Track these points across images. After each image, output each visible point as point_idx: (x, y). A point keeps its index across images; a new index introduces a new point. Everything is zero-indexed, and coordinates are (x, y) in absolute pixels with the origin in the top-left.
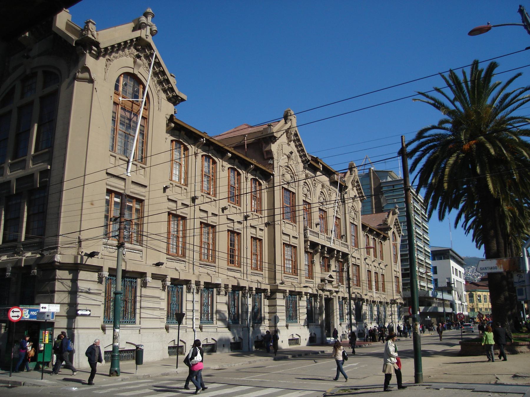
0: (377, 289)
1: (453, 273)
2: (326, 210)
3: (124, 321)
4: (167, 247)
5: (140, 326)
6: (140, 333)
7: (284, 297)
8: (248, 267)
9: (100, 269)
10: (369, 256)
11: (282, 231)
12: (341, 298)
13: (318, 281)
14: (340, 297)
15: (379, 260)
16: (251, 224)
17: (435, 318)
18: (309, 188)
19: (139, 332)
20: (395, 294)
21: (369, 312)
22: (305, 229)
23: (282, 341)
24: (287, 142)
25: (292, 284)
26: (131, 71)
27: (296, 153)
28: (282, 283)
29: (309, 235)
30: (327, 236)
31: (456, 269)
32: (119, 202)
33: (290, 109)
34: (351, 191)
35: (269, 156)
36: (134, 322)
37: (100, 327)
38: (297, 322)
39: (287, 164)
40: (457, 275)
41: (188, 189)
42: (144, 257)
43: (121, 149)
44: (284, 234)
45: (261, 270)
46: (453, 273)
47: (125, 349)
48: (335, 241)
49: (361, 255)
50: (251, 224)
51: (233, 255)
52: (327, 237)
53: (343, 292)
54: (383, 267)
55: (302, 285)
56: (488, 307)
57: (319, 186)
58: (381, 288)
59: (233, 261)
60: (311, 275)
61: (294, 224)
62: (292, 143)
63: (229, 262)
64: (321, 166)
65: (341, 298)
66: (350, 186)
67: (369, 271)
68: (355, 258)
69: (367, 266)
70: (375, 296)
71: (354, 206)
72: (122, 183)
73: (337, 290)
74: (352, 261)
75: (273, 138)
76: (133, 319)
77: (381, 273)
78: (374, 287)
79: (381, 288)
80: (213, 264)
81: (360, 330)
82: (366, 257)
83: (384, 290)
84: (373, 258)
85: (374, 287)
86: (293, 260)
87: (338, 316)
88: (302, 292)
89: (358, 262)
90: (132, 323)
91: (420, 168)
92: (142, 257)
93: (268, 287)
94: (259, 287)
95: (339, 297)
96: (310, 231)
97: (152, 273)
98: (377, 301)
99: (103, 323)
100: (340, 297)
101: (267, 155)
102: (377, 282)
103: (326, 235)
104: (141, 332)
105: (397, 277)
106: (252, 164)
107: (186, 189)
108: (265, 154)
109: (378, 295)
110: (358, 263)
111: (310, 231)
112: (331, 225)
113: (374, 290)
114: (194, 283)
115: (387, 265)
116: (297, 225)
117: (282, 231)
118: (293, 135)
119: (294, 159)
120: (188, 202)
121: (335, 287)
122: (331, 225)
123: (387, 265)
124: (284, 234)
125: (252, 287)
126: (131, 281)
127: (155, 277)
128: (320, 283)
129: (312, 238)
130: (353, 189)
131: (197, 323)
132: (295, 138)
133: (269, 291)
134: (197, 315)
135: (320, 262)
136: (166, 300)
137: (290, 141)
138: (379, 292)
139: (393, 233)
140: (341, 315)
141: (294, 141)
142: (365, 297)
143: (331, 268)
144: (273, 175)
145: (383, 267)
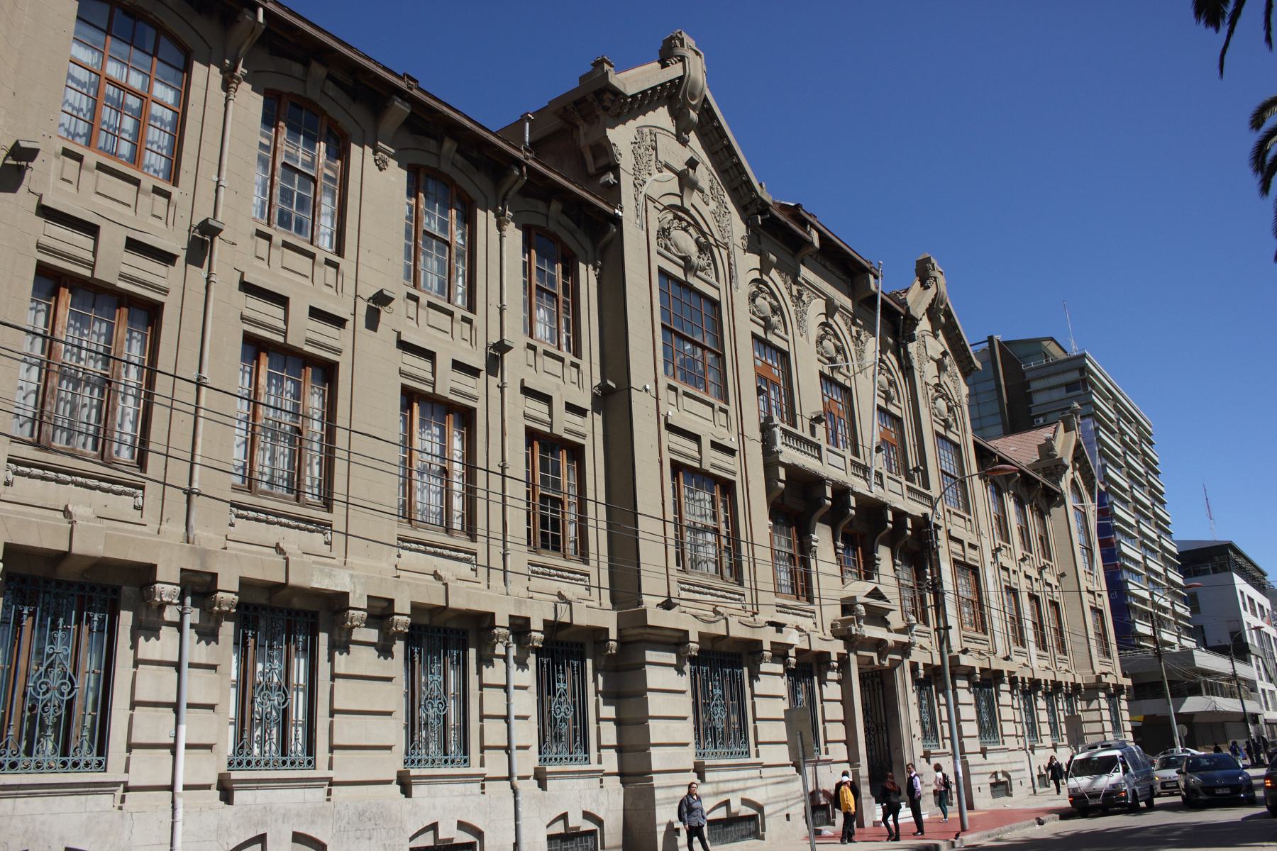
0: (1042, 644)
1: (1245, 609)
2: (848, 384)
4: (529, 530)
5: (482, 771)
6: (602, 787)
8: (197, 468)
10: (1006, 544)
11: (666, 419)
12: (921, 666)
13: (833, 613)
14: (917, 663)
15: (1037, 557)
16: (523, 381)
17: (612, 705)
18: (841, 342)
19: (599, 785)
20: (1096, 660)
21: (1023, 713)
22: (766, 428)
25: (715, 611)
26: (677, 201)
27: (705, 174)
28: (668, 605)
29: (779, 446)
30: (855, 459)
31: (1251, 600)
32: (818, 524)
33: (928, 255)
34: (930, 340)
35: (602, 162)
36: (465, 761)
37: (532, 773)
38: (748, 754)
39: (936, 381)
40: (1254, 613)
41: (478, 319)
42: (819, 624)
44: (672, 428)
45: (583, 555)
46: (1245, 609)
48: (885, 478)
49: (979, 535)
50: (523, 381)
51: (555, 523)
52: (909, 488)
53: (925, 652)
54: (1053, 580)
55: (763, 618)
56: (258, 423)
57: (818, 306)
58: (1051, 640)
59: (556, 539)
60: (803, 587)
61: (967, 516)
64: (815, 235)
65: (921, 666)
66: (924, 325)
67: (1012, 591)
68: (960, 542)
69: (1004, 574)
70: (1035, 666)
71: (942, 383)
73: (904, 638)
74: (951, 552)
76: (94, 758)
77: (1048, 598)
78: (1030, 634)
79: (1051, 640)
80: (322, 515)
82: (997, 546)
83: (1062, 647)
84: (1019, 552)
85: (1030, 634)
86: (723, 533)
87: (917, 730)
88: (759, 642)
89: (973, 557)
90: (266, 765)
92: (815, 624)
93: (608, 620)
94: (565, 618)
95: (914, 666)
96: (785, 432)
97: (182, 570)
99: (224, 769)
100: (917, 663)
101: (595, 157)
102: (1039, 625)
103: (905, 483)
104: (486, 790)
105: (1097, 612)
106: (519, 163)
107: (167, 195)
108: (589, 158)
109: (1045, 663)
110: (971, 559)
111: (785, 432)
112: (870, 430)
113: (1032, 646)
114: (541, 627)
115: (1063, 575)
116: (732, 409)
117: (666, 419)
119: (707, 191)
120: (479, 362)
121: (898, 631)
122: (870, 430)
123: (1063, 575)
124: (672, 428)
125: (493, 614)
128: (840, 617)
129: (790, 455)
131: (527, 762)
133: (613, 634)
134: (527, 733)
139: (1073, 482)
140: (928, 726)
142: (768, 637)
143: (880, 567)
144: (618, 221)
145: (1053, 580)
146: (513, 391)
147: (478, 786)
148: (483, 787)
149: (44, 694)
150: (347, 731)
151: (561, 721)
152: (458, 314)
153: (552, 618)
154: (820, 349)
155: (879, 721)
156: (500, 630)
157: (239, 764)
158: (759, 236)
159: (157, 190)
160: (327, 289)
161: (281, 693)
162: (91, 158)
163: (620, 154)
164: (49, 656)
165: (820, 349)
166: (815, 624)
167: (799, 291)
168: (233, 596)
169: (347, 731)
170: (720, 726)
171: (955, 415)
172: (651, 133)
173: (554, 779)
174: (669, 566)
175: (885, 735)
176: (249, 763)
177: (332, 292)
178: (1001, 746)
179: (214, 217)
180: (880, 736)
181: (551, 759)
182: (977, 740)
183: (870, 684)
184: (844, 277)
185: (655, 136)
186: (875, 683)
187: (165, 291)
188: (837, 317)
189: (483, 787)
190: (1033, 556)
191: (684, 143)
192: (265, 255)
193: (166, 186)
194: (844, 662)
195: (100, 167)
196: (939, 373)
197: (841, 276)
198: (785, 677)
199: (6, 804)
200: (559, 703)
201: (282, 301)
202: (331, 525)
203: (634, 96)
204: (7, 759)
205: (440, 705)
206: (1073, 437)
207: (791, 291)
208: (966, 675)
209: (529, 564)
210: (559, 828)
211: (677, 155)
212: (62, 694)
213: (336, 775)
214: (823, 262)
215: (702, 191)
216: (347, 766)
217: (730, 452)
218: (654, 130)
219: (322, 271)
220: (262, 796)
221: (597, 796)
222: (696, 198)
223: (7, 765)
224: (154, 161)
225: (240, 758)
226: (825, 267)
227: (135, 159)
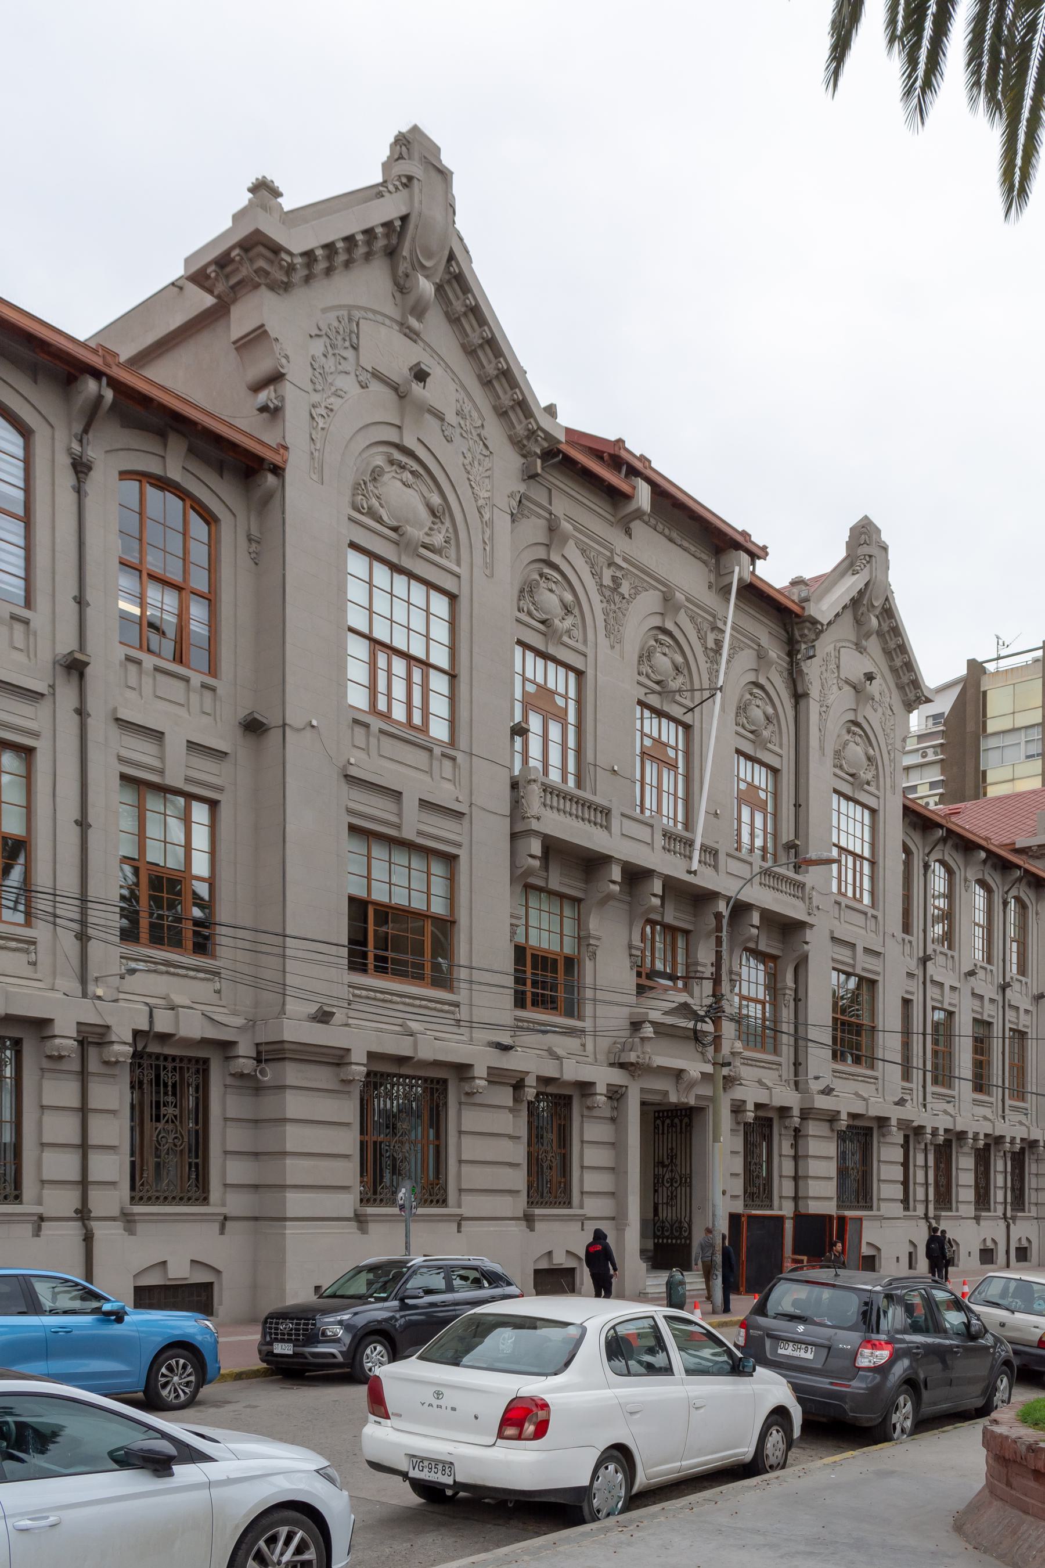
0: (980, 1084)
3: (435, 1198)
7: (516, 1100)
9: (342, 1057)
14: (937, 1128)
23: (898, 1258)
24: (854, 639)
26: (392, 436)
41: (39, 618)
42: (880, 1089)
43: (182, 616)
47: (563, 1266)
54: (1025, 1003)
62: (873, 645)
63: (929, 1075)
72: (390, 805)
75: (808, 624)
81: (985, 1240)
91: (829, 46)
92: (877, 1090)
98: (1013, 1139)
114: (604, 1092)
118: (877, 612)
119: (451, 417)
126: (432, 1089)
127: (496, 1077)
130: (860, 648)
132: (885, 627)
135: (630, 947)
136: (742, 1154)
137: (868, 636)
138: (992, 1100)
140: (982, 1191)
141: (880, 634)
146: (99, 726)
147: (455, 1226)
148: (459, 1226)
150: (473, 1177)
151: (168, 1154)
152: (196, 679)
153: (145, 1027)
154: (645, 669)
155: (683, 1172)
157: (532, 1203)
158: (550, 491)
163: (286, 357)
165: (645, 669)
166: (877, 1090)
167: (614, 579)
169: (473, 1177)
171: (877, 768)
172: (350, 320)
175: (688, 1189)
177: (21, 657)
178: (953, 1214)
179: (81, 650)
180: (683, 1189)
181: (174, 1198)
182: (972, 1207)
183: (678, 1124)
184: (704, 557)
185: (358, 325)
186: (666, 1124)
187: (36, 735)
188: (572, 551)
189: (459, 1226)
190: (994, 968)
191: (412, 335)
193: (25, 613)
194: (616, 1095)
196: (857, 705)
197: (698, 554)
200: (402, 1143)
201: (158, 736)
203: (309, 255)
207: (705, 642)
208: (829, 1121)
209: (121, 957)
210: (544, 1265)
211: (855, 665)
213: (465, 1211)
214: (667, 531)
215: (440, 417)
216: (471, 1205)
217: (877, 954)
218: (357, 314)
219: (150, 681)
222: (869, 712)
225: (432, 1198)
226: (671, 540)
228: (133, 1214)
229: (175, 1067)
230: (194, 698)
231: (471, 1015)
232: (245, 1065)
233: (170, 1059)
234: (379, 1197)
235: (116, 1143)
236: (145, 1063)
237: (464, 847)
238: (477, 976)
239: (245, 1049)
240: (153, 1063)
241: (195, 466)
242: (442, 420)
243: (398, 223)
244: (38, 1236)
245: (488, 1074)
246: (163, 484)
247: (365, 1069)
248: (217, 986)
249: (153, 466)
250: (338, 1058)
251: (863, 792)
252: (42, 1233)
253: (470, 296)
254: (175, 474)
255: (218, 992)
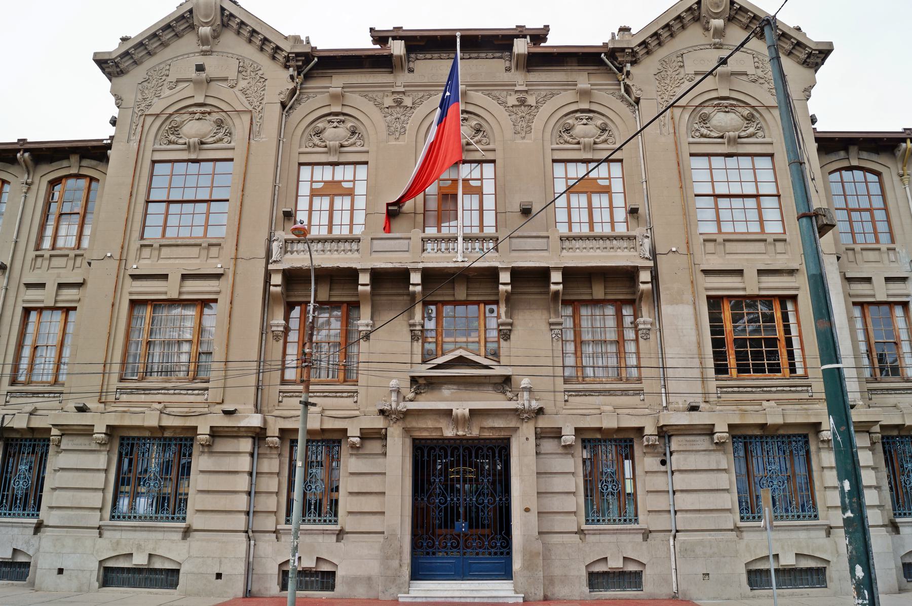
107: (894, 249)
149: (310, 490)
156: (567, 437)
157: (156, 518)
159: (889, 249)
160: (893, 265)
161: (615, 484)
162: (858, 248)
164: (311, 474)
168: (726, 434)
170: (610, 497)
173: (109, 530)
174: (69, 392)
176: (625, 520)
192: (853, 260)
193: (892, 246)
195: (862, 249)
198: (730, 448)
199: (4, 530)
202: (643, 390)
204: (3, 511)
205: (614, 487)
206: (534, 97)
212: (780, 486)
219: (860, 255)
220: (117, 535)
221: (29, 540)
223: (3, 514)
224: (884, 238)
227: (877, 241)
228: (741, 527)
229: (627, 445)
230: (885, 256)
231: (555, 396)
232: (654, 440)
233: (15, 440)
234: (322, 519)
235: (728, 488)
236: (125, 442)
237: (21, 300)
238: (549, 371)
239: (650, 430)
240: (183, 443)
241: (865, 155)
242: (747, 75)
243: (695, 6)
244: (829, 537)
245: (361, 433)
246: (850, 168)
247: (880, 435)
248: (355, 399)
249: (845, 164)
250: (709, 431)
251: (739, 145)
252: (831, 536)
253: (157, 33)
254: (855, 163)
255: (356, 402)
